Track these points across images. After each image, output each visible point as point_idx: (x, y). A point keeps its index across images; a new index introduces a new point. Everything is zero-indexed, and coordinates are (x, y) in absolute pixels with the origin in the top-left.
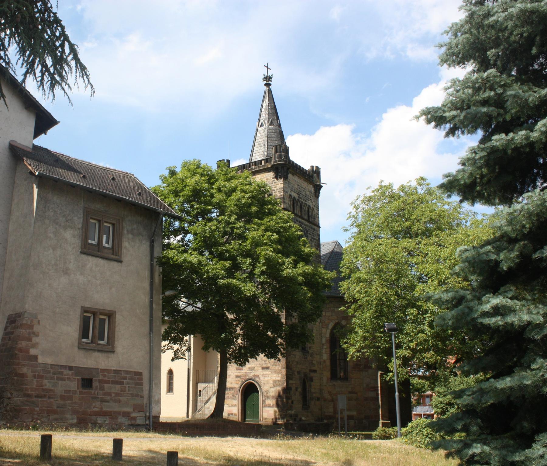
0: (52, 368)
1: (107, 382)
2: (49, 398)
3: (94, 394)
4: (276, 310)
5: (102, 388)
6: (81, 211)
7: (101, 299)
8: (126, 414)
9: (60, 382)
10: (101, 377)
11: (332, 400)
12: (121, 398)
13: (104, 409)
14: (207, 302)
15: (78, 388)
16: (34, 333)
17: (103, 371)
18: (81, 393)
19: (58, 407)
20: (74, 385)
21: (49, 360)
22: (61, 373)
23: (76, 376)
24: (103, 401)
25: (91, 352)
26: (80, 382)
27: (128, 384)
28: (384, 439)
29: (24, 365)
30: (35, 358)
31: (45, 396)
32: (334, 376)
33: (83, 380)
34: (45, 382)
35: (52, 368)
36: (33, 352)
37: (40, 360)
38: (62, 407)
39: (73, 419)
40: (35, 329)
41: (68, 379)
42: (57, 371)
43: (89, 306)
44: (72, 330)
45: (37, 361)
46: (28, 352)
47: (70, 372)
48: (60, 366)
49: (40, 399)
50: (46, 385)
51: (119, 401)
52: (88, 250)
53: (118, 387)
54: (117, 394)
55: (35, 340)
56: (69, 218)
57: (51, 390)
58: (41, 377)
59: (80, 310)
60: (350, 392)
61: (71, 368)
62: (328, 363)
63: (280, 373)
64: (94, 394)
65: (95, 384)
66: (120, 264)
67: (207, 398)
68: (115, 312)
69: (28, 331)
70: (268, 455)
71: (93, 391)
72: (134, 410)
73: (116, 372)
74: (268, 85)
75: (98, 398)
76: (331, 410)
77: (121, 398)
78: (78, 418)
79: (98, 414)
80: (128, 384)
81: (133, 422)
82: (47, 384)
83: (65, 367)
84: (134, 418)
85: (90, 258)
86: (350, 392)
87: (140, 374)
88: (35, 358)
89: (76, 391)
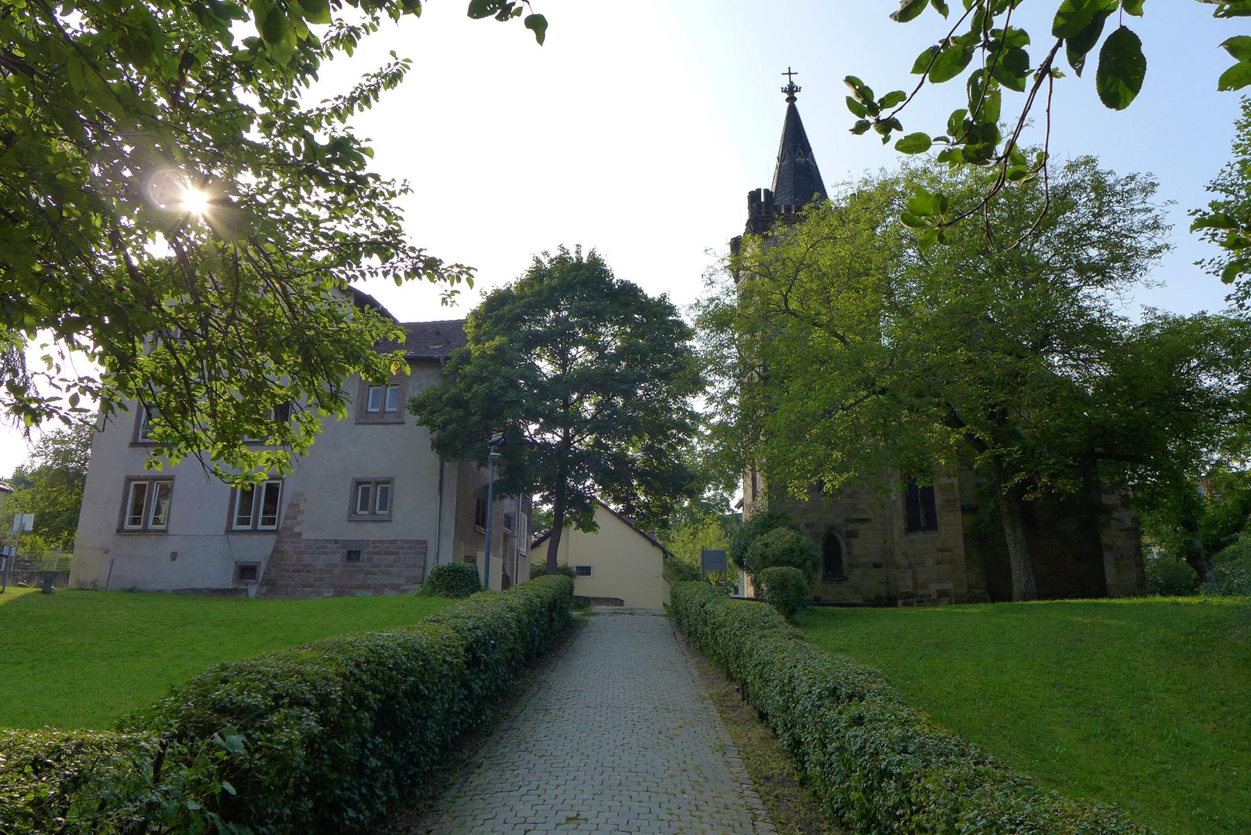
4: (814, 431)
5: (370, 560)
7: (375, 468)
10: (371, 549)
11: (910, 566)
20: (337, 558)
24: (368, 573)
28: (876, 606)
30: (300, 534)
32: (913, 525)
36: (297, 529)
42: (321, 546)
44: (342, 504)
47: (335, 546)
48: (922, 601)
60: (939, 550)
61: (336, 542)
62: (900, 505)
63: (32, 509)
65: (363, 556)
67: (854, 601)
74: (792, 99)
76: (910, 583)
82: (307, 558)
83: (329, 541)
86: (939, 550)
87: (425, 542)
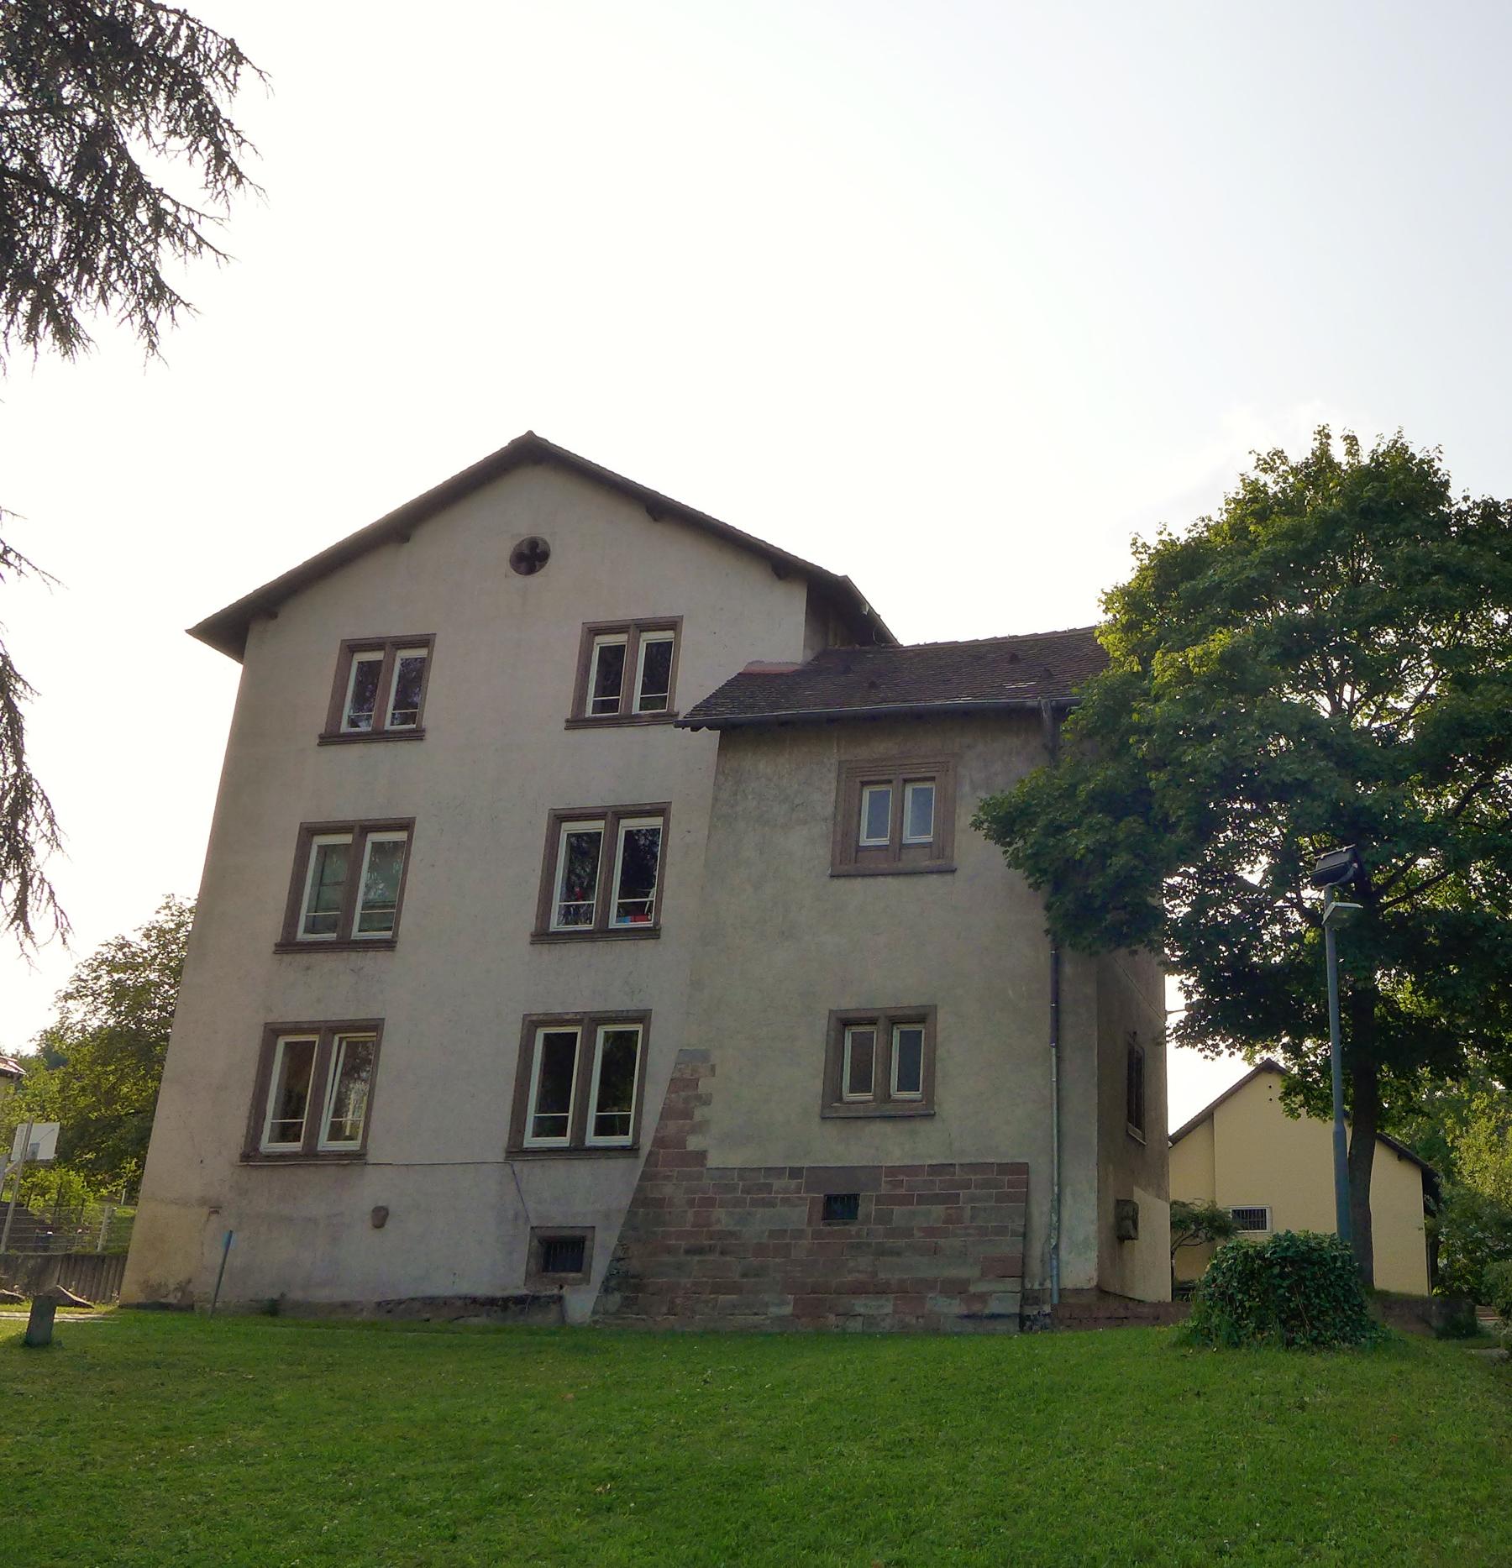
0: (741, 1178)
1: (905, 1200)
2: (722, 1253)
3: (858, 1235)
6: (833, 775)
7: (884, 984)
8: (956, 1288)
9: (760, 1212)
10: (885, 1189)
12: (941, 1241)
13: (882, 1276)
14: (1185, 933)
15: (810, 1222)
16: (699, 1098)
17: (893, 1171)
18: (817, 1235)
19: (744, 1275)
20: (799, 1215)
21: (735, 1159)
22: (768, 1187)
23: (807, 1191)
24: (881, 1252)
25: (860, 1123)
26: (820, 1208)
27: (973, 1199)
29: (667, 1178)
30: (701, 1156)
31: (711, 1249)
33: (830, 1200)
34: (719, 1213)
35: (741, 1178)
36: (694, 1143)
37: (714, 1161)
38: (757, 1275)
39: (783, 1303)
40: (703, 1087)
41: (786, 1201)
42: (756, 1185)
43: (853, 1006)
44: (804, 1074)
45: (703, 1165)
46: (682, 1144)
49: (697, 1258)
50: (719, 1221)
51: (936, 1251)
52: (850, 862)
53: (938, 1210)
54: (930, 1232)
55: (699, 1113)
56: (797, 801)
57: (732, 1234)
58: (709, 1202)
59: (825, 1022)
61: (795, 1173)
64: (858, 1235)
65: (867, 1208)
66: (949, 877)
68: (936, 1007)
69: (683, 1094)
70: (1315, 1359)
71: (854, 1229)
72: (984, 1274)
73: (936, 1169)
75: (869, 1245)
77: (941, 1241)
78: (796, 1302)
79: (859, 1290)
80: (973, 1199)
81: (976, 1308)
82: (722, 1218)
83: (778, 1172)
84: (982, 1297)
85: (858, 884)
87: (1022, 1169)
88: (701, 1156)
89: (802, 1231)
